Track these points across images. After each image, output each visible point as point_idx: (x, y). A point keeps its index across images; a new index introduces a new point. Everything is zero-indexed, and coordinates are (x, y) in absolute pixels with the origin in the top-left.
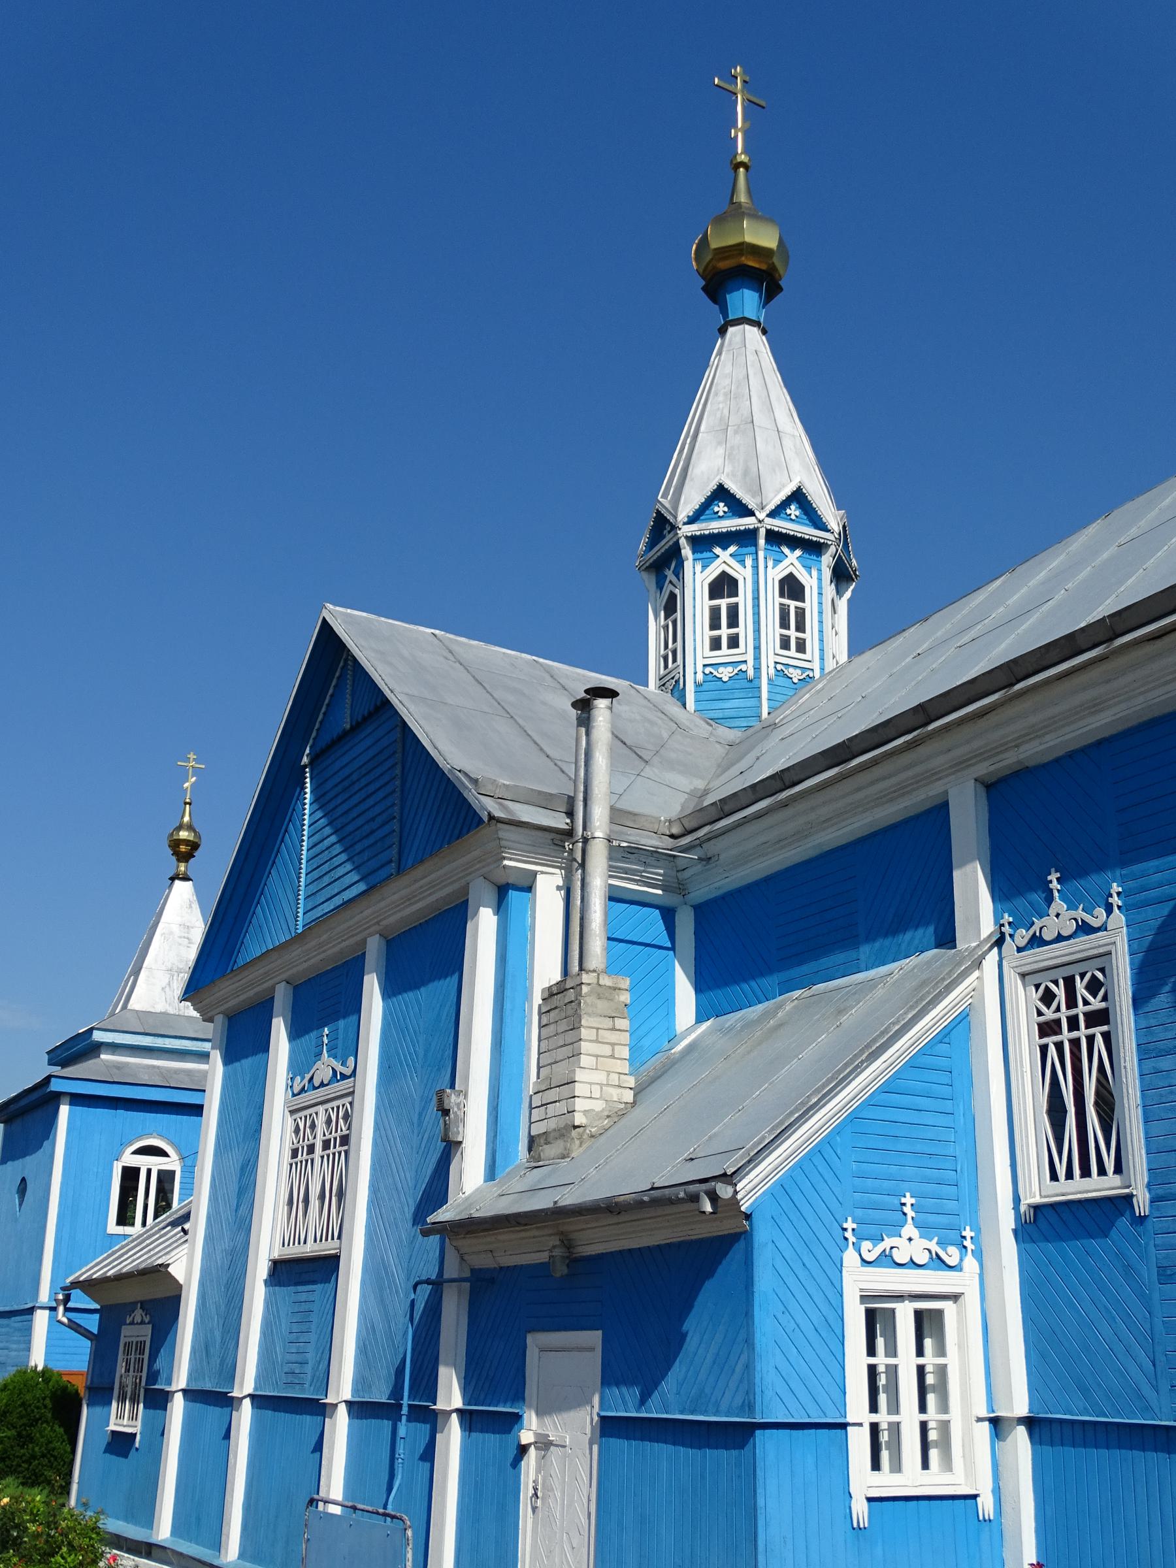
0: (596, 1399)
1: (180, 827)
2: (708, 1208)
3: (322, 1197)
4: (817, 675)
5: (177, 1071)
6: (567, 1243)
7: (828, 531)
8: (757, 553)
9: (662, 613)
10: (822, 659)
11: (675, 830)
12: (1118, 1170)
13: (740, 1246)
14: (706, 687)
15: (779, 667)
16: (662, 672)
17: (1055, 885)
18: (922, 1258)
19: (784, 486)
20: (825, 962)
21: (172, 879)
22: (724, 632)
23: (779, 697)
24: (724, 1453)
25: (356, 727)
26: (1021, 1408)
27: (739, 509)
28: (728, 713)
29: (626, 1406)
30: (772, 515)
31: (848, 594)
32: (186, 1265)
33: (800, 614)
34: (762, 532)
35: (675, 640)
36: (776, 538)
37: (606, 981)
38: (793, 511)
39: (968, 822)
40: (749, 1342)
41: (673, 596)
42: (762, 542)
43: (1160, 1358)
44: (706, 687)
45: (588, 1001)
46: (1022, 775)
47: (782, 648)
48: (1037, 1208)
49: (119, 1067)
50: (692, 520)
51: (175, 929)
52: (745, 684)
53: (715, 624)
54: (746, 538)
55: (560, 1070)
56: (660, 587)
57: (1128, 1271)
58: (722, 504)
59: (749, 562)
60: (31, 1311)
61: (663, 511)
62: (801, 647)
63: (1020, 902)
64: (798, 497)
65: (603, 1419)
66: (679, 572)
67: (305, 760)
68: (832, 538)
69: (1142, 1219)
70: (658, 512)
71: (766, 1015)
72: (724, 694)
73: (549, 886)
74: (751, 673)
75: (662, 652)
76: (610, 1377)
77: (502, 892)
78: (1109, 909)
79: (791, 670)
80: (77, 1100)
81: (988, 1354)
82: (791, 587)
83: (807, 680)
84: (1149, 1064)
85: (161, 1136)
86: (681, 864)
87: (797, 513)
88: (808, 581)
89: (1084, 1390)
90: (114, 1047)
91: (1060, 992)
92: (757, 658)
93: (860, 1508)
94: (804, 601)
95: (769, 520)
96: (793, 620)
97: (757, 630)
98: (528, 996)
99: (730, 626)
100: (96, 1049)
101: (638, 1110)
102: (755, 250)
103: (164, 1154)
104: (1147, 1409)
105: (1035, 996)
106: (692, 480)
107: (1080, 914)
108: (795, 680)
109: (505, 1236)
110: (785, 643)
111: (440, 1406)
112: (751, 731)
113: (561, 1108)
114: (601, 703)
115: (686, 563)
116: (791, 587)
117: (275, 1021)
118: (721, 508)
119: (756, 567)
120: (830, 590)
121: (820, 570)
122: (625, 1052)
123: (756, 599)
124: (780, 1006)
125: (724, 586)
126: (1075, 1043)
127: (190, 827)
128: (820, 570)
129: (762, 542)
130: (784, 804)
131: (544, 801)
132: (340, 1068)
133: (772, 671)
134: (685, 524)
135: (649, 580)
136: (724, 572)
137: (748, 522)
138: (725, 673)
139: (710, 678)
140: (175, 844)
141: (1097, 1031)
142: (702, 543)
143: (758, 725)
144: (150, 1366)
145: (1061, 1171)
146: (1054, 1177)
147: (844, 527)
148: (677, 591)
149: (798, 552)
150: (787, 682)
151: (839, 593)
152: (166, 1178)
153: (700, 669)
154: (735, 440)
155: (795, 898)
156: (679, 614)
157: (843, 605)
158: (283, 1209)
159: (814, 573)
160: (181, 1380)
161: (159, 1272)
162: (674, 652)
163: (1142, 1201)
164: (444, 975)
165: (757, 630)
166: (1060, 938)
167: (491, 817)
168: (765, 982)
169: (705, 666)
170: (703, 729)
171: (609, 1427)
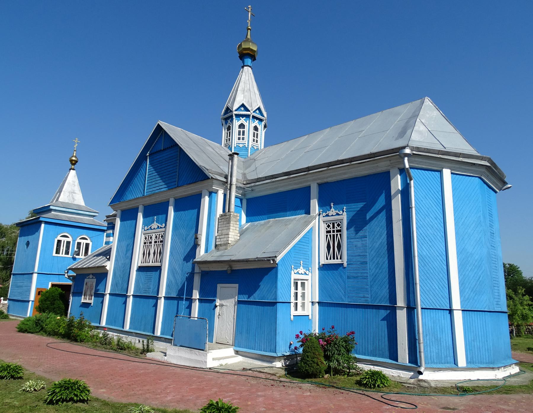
0: (236, 297)
1: (73, 157)
2: (272, 262)
3: (154, 253)
5: (72, 217)
6: (231, 267)
11: (244, 183)
12: (341, 258)
13: (274, 270)
17: (332, 205)
18: (303, 273)
20: (279, 214)
21: (70, 169)
24: (269, 307)
25: (164, 150)
26: (317, 300)
27: (247, 110)
29: (244, 298)
32: (110, 266)
36: (254, 117)
37: (235, 214)
38: (257, 112)
39: (314, 191)
40: (276, 287)
41: (229, 127)
42: (251, 118)
43: (346, 292)
45: (232, 218)
46: (327, 183)
48: (323, 265)
49: (57, 215)
50: (236, 110)
51: (71, 182)
53: (239, 134)
54: (248, 116)
55: (225, 232)
57: (341, 276)
59: (248, 122)
60: (32, 274)
62: (257, 142)
63: (324, 208)
64: (259, 109)
65: (238, 301)
66: (232, 121)
67: (148, 154)
69: (345, 268)
71: (265, 223)
73: (221, 193)
76: (240, 293)
77: (210, 194)
78: (343, 211)
80: (46, 223)
81: (312, 290)
82: (256, 128)
84: (349, 240)
85: (68, 233)
86: (246, 190)
89: (330, 297)
90: (55, 210)
91: (331, 226)
93: (292, 317)
96: (256, 135)
98: (216, 215)
100: (51, 210)
101: (240, 242)
102: (252, 50)
103: (86, 239)
104: (343, 300)
105: (326, 226)
107: (337, 211)
109: (214, 265)
110: (254, 140)
111: (193, 298)
113: (225, 239)
114: (236, 156)
116: (256, 128)
117: (139, 214)
118: (242, 109)
119: (249, 123)
122: (238, 229)
124: (269, 222)
125: (242, 126)
126: (334, 235)
127: (75, 157)
130: (273, 182)
131: (220, 175)
132: (160, 226)
135: (224, 122)
138: (241, 145)
140: (71, 161)
141: (339, 233)
142: (238, 116)
144: (96, 287)
145: (329, 258)
146: (327, 259)
152: (68, 243)
154: (246, 94)
155: (270, 201)
156: (231, 131)
158: (141, 255)
160: (108, 291)
161: (104, 267)
162: (229, 139)
163: (345, 264)
164: (193, 208)
166: (332, 215)
167: (212, 178)
168: (263, 216)
171: (239, 302)
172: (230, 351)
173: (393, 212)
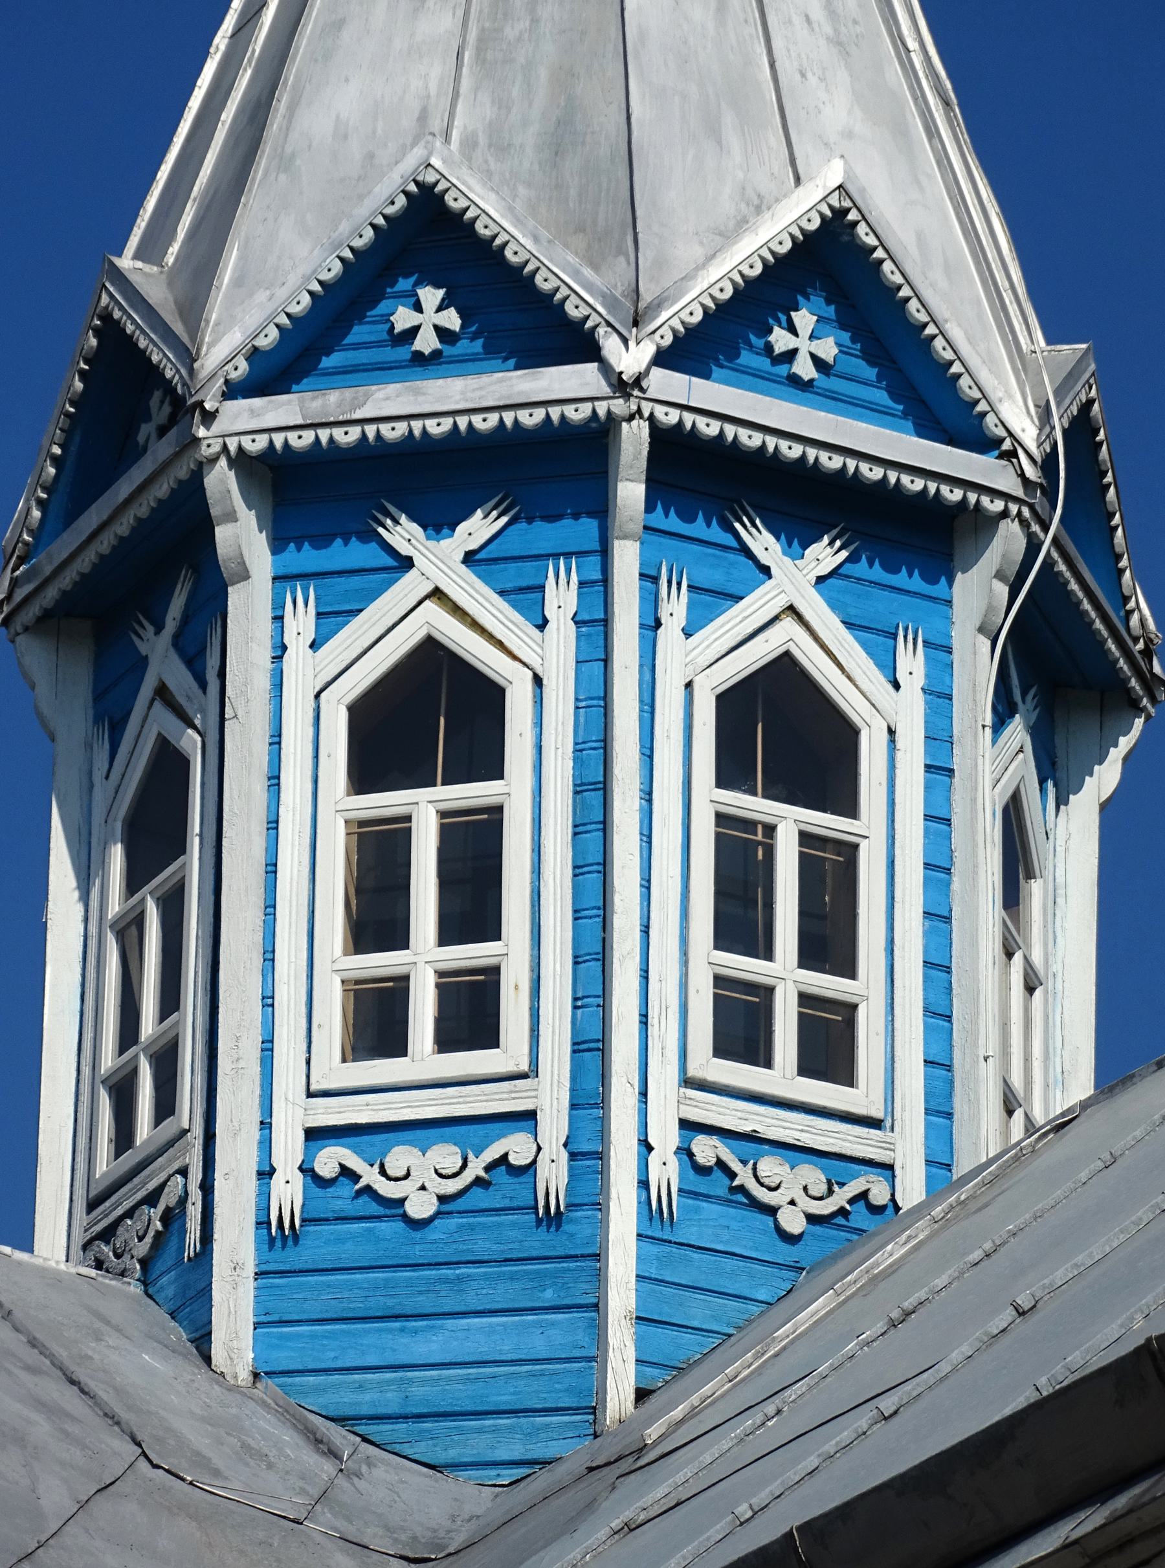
4: (912, 1188)
7: (983, 443)
8: (605, 553)
9: (117, 856)
10: (940, 1110)
14: (318, 1246)
15: (706, 1149)
16: (104, 1164)
19: (761, 206)
22: (424, 959)
23: (698, 1311)
27: (522, 319)
28: (425, 1390)
30: (688, 352)
31: (1106, 777)
33: (831, 874)
34: (634, 442)
35: (170, 1001)
36: (708, 479)
38: (807, 335)
41: (169, 767)
42: (630, 493)
44: (318, 1246)
47: (723, 1049)
50: (271, 373)
52: (519, 1235)
53: (377, 918)
56: (111, 719)
58: (431, 296)
59: (562, 598)
61: (132, 323)
62: (829, 1044)
64: (832, 263)
68: (1008, 483)
70: (110, 330)
72: (411, 1291)
74: (554, 1175)
75: (109, 1060)
79: (771, 1167)
82: (784, 733)
83: (855, 1222)
87: (828, 349)
88: (881, 702)
92: (589, 1102)
94: (851, 810)
95: (668, 384)
96: (786, 906)
97: (593, 957)
99: (452, 931)
106: (285, 163)
108: (793, 1222)
110: (742, 1025)
112: (543, 1480)
115: (236, 596)
116: (784, 733)
118: (428, 313)
119: (595, 626)
120: (997, 761)
121: (939, 650)
123: (593, 788)
125: (426, 718)
128: (939, 650)
129: (630, 493)
133: (666, 1170)
134: (232, 391)
135: (52, 683)
136: (430, 647)
137: (567, 386)
138: (421, 1177)
139: (341, 1198)
143: (575, 1452)
147: (1081, 430)
148: (190, 742)
149: (824, 555)
150: (747, 1233)
151: (1057, 770)
153: (288, 1149)
156: (194, 863)
157: (1072, 842)
159: (912, 664)
162: (166, 1062)
165: (593, 957)
169: (315, 1135)
170: (287, 1467)
172: (1137, 720)
173: (37, 1216)
